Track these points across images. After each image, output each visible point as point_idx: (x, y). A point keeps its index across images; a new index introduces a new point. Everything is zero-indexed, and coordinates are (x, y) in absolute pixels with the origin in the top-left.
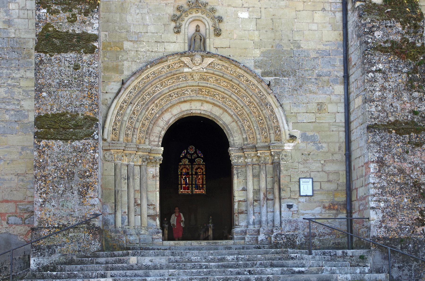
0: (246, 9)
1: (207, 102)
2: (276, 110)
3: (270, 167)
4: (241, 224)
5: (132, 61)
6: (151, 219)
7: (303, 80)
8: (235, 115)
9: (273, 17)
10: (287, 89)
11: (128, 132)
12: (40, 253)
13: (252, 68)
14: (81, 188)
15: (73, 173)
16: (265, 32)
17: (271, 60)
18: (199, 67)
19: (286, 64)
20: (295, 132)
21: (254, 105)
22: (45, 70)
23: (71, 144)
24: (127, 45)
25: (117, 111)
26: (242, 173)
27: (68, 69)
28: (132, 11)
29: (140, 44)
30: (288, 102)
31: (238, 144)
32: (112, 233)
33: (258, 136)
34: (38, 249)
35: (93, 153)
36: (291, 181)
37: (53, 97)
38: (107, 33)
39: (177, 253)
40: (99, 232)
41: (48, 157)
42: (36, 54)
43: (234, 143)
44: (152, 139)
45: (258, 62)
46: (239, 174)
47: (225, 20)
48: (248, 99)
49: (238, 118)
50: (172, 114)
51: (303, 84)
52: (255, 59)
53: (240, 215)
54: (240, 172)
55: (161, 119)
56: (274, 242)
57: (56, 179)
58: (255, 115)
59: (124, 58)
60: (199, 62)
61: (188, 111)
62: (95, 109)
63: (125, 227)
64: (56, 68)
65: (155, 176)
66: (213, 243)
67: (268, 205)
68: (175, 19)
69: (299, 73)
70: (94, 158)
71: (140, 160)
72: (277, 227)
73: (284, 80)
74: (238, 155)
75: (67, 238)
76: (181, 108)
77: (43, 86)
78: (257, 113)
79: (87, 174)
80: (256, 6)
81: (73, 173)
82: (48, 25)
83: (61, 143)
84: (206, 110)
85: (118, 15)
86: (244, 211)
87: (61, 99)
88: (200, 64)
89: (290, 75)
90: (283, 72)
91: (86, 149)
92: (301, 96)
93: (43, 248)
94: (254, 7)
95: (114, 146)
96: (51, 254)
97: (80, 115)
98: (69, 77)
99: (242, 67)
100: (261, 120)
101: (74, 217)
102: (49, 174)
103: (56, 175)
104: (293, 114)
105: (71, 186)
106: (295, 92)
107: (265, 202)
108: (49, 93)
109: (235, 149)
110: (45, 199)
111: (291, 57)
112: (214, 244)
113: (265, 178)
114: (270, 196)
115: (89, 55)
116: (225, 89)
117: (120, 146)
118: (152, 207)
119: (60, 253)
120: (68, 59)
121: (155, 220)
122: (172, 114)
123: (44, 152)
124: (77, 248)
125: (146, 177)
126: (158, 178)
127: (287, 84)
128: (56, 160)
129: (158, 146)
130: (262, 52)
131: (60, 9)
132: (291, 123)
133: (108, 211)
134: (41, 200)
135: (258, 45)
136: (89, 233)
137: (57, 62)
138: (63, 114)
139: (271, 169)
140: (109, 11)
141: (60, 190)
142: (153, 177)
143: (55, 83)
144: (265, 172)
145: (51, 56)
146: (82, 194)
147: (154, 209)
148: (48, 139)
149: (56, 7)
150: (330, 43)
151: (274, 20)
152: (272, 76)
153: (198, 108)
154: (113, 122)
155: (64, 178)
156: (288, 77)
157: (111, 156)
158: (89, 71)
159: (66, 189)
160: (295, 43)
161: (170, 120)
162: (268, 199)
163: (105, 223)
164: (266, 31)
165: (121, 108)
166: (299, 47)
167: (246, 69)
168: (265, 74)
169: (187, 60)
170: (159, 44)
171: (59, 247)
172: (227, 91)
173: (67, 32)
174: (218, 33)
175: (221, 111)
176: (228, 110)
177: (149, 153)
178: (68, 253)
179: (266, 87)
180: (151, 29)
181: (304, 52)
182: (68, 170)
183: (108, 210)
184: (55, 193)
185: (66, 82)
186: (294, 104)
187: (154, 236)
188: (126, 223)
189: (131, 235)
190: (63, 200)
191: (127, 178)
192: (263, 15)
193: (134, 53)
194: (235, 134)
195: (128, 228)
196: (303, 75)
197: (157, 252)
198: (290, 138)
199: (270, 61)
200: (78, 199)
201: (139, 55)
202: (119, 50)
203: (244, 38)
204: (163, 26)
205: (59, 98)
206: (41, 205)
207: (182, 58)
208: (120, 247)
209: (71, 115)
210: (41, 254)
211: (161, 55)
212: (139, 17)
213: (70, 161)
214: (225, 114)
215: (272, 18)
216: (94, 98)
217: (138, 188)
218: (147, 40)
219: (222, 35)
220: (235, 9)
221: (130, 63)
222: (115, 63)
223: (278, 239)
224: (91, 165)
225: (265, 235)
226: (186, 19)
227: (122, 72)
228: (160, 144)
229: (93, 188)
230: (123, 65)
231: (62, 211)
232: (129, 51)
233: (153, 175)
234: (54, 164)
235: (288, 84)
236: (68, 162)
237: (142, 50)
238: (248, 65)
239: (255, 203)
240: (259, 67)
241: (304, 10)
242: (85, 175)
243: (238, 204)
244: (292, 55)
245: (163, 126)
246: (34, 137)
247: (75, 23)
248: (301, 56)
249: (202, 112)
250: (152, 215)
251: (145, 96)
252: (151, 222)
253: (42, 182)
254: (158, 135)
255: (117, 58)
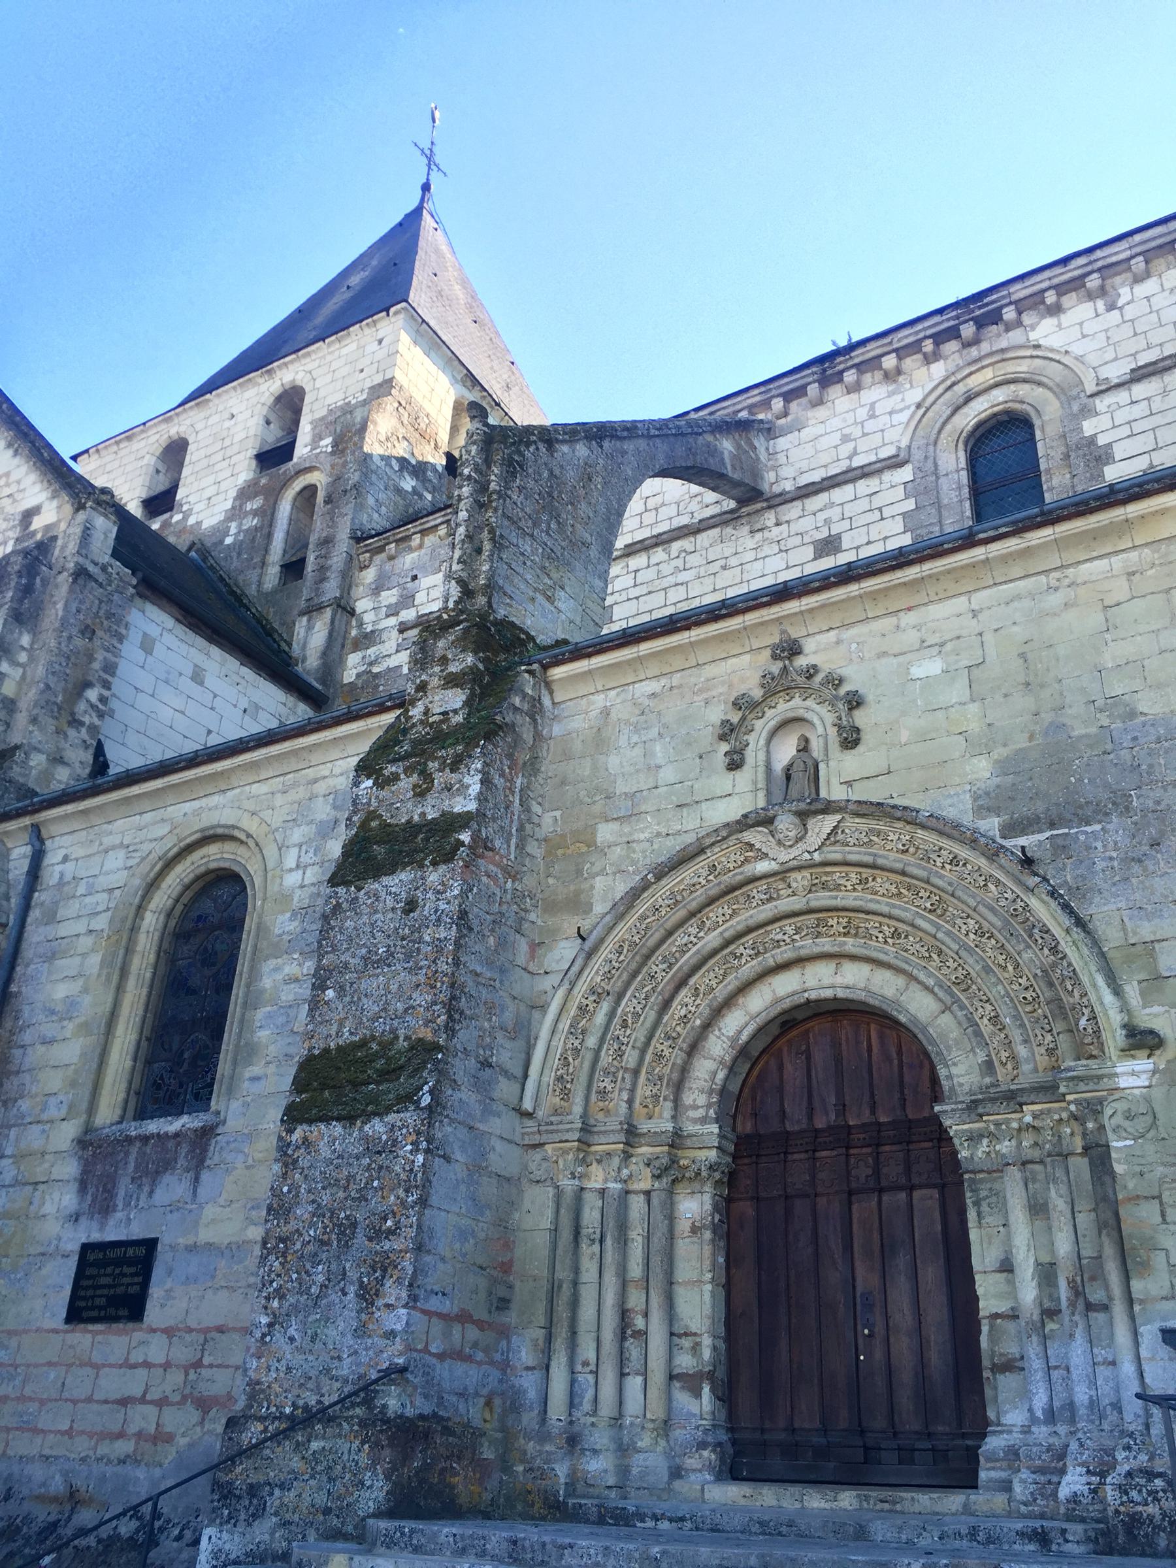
0: (935, 650)
1: (853, 958)
2: (1066, 946)
3: (1080, 1166)
4: (1008, 1416)
5: (614, 874)
6: (683, 1388)
7: (1163, 821)
8: (941, 987)
9: (1026, 648)
10: (1100, 865)
11: (604, 1084)
12: (226, 1512)
13: (967, 820)
14: (368, 1275)
15: (354, 1225)
16: (1002, 699)
17: (1031, 779)
18: (795, 852)
19: (1089, 780)
20: (1156, 1015)
21: (993, 942)
22: (340, 928)
23: (361, 1129)
24: (605, 832)
25: (569, 1022)
26: (994, 1199)
27: (390, 915)
28: (623, 741)
29: (638, 821)
30: (1114, 907)
31: (966, 1088)
32: (530, 1440)
33: (1022, 1051)
34: (226, 1497)
35: (411, 1152)
36: (1169, 1219)
37: (348, 999)
38: (558, 814)
39: (527, 1543)
40: (388, 1438)
41: (302, 1179)
42: (328, 890)
43: (952, 1089)
44: (688, 1098)
45: (987, 794)
46: (984, 1205)
47: (870, 697)
48: (972, 922)
49: (952, 995)
50: (747, 1013)
51: (1162, 833)
52: (974, 789)
53: (1000, 1378)
54: (987, 1197)
55: (717, 1033)
56: (1117, 1512)
57: (310, 1248)
58: (1006, 975)
59: (597, 868)
60: (792, 834)
61: (796, 997)
62: (439, 1016)
63: (582, 1420)
64: (365, 918)
65: (700, 1228)
66: (882, 1501)
67: (1094, 1330)
68: (728, 731)
69: (1142, 800)
70: (412, 1170)
71: (647, 1172)
72: (1131, 1435)
73: (1086, 833)
74: (970, 1131)
75: (303, 1458)
76: (773, 991)
77: (331, 972)
78: (1010, 968)
79: (389, 1223)
80: (964, 633)
81: (354, 1225)
82: (372, 815)
83: (337, 1129)
84: (851, 983)
85: (588, 763)
86: (1015, 1360)
87: (365, 1000)
88: (798, 840)
89: (1106, 814)
90: (1081, 807)
91: (395, 1142)
92: (1161, 876)
93: (237, 1492)
94: (958, 638)
95: (552, 1132)
96: (254, 1516)
97: (401, 1039)
98: (389, 936)
99: (925, 820)
100: (1026, 989)
101: (337, 1381)
102: (297, 1230)
103: (312, 1233)
104: (1139, 948)
105: (344, 1268)
106: (1136, 868)
107: (1077, 1318)
108: (341, 990)
109: (953, 1110)
110: (275, 1315)
111: (1105, 753)
112: (886, 1506)
113: (1069, 1216)
114: (1096, 1295)
115: (442, 868)
116: (894, 906)
117: (567, 1131)
118: (687, 1343)
119: (276, 1514)
120: (393, 890)
121: (698, 1395)
122: (747, 1013)
123: (296, 1161)
124: (321, 1499)
125: (665, 1230)
126: (708, 1235)
127: (1099, 845)
128: (320, 1186)
129: (704, 1120)
130: (997, 762)
131: (400, 771)
132: (1135, 983)
133: (524, 1359)
134: (264, 1320)
135: (977, 746)
136: (363, 1443)
137: (369, 901)
138: (363, 1043)
139: (1086, 1175)
140: (567, 756)
141: (314, 1283)
142: (694, 1230)
143: (356, 961)
144: (1063, 1189)
145: (359, 889)
146: (368, 1296)
147: (696, 1349)
148: (310, 1122)
149: (394, 769)
150: (960, 1106)
151: (1030, 656)
152: (1040, 831)
153: (826, 981)
154: (558, 1056)
155: (328, 1243)
156: (1100, 822)
157: (545, 1164)
158: (436, 911)
159: (329, 1280)
160: (1115, 705)
161: (740, 1032)
162: (1089, 1307)
163: (513, 1402)
164: (1006, 696)
165: (582, 1009)
166: (1132, 714)
167: (940, 826)
168: (1012, 829)
169: (759, 837)
170: (685, 810)
171: (277, 1492)
172: (900, 908)
173: (409, 822)
174: (851, 739)
175: (901, 981)
176: (915, 972)
177: (671, 1146)
178: (296, 1516)
179: (1016, 868)
180: (668, 774)
181: (1153, 725)
182: (342, 1215)
183: (523, 1354)
184: (301, 1294)
185: (380, 951)
186: (1136, 912)
187: (689, 1461)
188: (587, 1406)
189: (595, 1452)
190: (318, 1316)
191: (598, 1236)
192: (991, 652)
193: (622, 849)
194: (954, 1054)
195: (593, 1424)
196: (1158, 803)
197: (462, 1536)
198: (1131, 1041)
199: (1029, 784)
200: (354, 1314)
201: (634, 852)
202: (584, 849)
203: (934, 735)
204: (698, 760)
205: (359, 999)
206: (264, 1335)
207: (745, 834)
208: (546, 1498)
209: (379, 1044)
210: (230, 1517)
211: (690, 838)
212: (638, 751)
213: (352, 1186)
214: (914, 986)
215: (1020, 651)
216: (439, 985)
217: (635, 1270)
218: (655, 808)
219: (862, 741)
220: (901, 659)
221: (610, 878)
222: (572, 888)
223: (1134, 1494)
224: (401, 1193)
225: (1088, 1472)
226: (759, 724)
227: (588, 909)
228: (712, 1113)
229: (396, 1274)
230: (592, 887)
231: (310, 1358)
232: (609, 847)
233: (693, 1223)
234: (313, 1197)
235: (1104, 846)
236: (346, 1188)
237: (642, 836)
238: (950, 813)
239: (1050, 1326)
240: (989, 809)
241: (1133, 598)
242: (384, 1228)
243: (992, 1326)
244: (1109, 747)
245: (722, 1053)
246: (282, 1120)
247: (428, 797)
248: (1142, 741)
249: (841, 994)
250: (687, 1375)
251: (654, 967)
252: (682, 1399)
253: (277, 1258)
254: (707, 1085)
255: (579, 872)
